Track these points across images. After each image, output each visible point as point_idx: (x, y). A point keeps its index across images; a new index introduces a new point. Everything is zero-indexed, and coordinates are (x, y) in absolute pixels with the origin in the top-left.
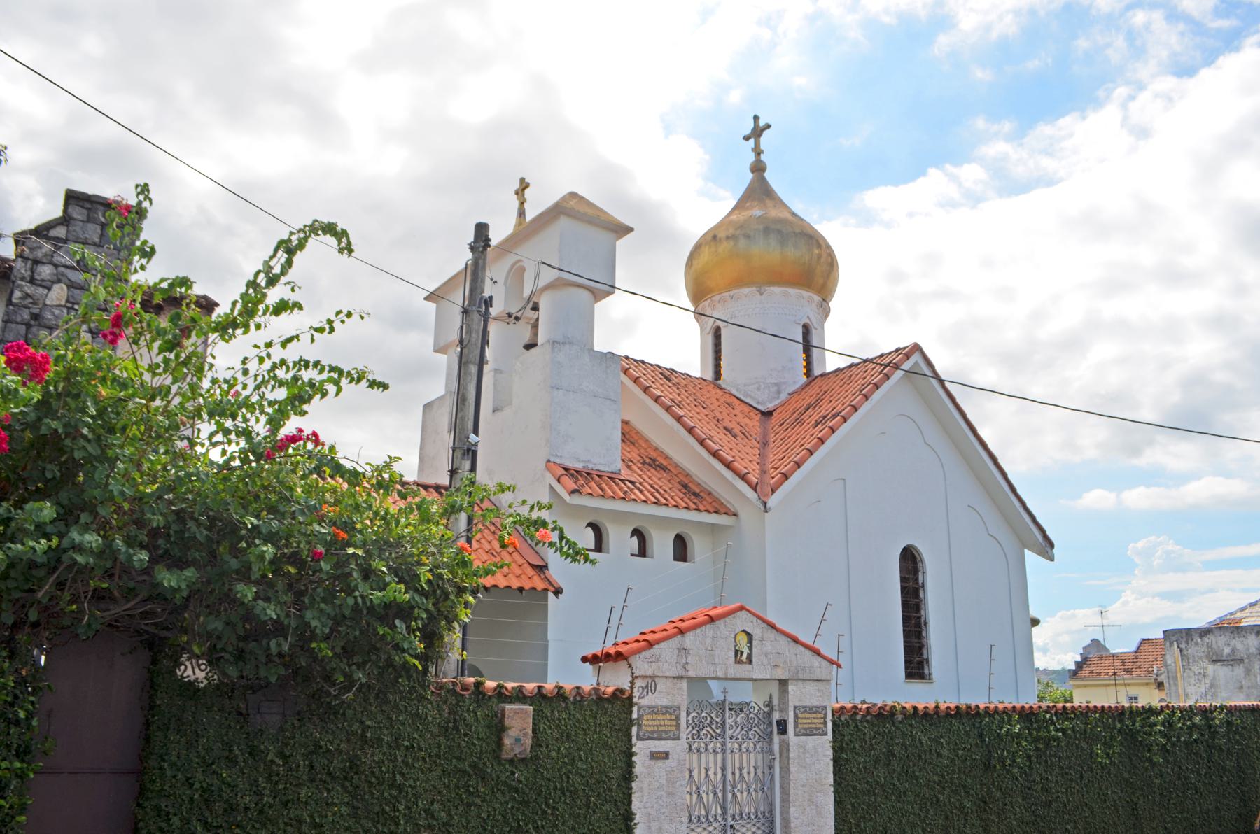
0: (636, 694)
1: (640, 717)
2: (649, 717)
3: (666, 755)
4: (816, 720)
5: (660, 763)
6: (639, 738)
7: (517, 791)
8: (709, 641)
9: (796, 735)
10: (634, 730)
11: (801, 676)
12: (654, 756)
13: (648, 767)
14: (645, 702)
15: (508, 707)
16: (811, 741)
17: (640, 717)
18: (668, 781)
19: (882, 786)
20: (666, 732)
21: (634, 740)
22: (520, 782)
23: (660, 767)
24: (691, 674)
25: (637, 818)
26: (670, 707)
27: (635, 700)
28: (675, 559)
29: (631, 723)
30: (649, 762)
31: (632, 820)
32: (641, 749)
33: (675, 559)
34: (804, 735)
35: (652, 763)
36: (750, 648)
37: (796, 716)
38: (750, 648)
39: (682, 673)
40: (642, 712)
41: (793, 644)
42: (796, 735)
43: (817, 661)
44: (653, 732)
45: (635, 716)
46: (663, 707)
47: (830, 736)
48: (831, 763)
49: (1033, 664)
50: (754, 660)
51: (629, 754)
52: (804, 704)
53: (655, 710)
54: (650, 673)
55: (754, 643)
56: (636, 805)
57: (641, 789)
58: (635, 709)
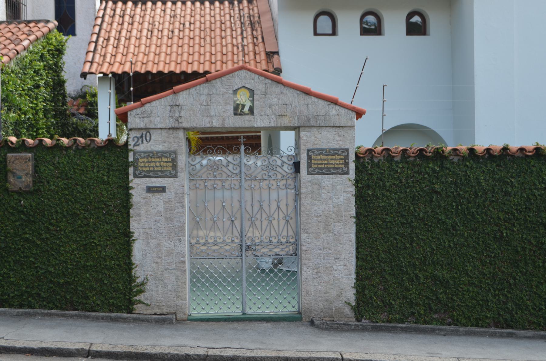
0: (131, 143)
1: (136, 160)
2: (145, 160)
3: (162, 189)
4: (337, 161)
5: (158, 196)
6: (136, 176)
7: (23, 212)
8: (203, 98)
9: (309, 173)
10: (131, 170)
11: (313, 123)
12: (150, 189)
13: (146, 198)
14: (142, 148)
15: (9, 155)
16: (327, 180)
17: (136, 160)
18: (166, 209)
19: (422, 219)
20: (162, 171)
21: (131, 177)
22: (25, 207)
23: (157, 199)
24: (185, 125)
25: (135, 236)
26: (166, 152)
27: (130, 147)
28: (361, 34)
29: (127, 165)
30: (145, 194)
31: (130, 237)
32: (138, 186)
33: (361, 34)
34: (318, 173)
35: (150, 195)
36: (253, 101)
37: (309, 158)
38: (253, 101)
39: (177, 125)
40: (137, 156)
41: (302, 96)
42: (309, 173)
43: (333, 110)
44: (149, 172)
45: (131, 159)
46: (157, 152)
47: (352, 175)
48: (353, 199)
49: (282, 130)
50: (255, 111)
51: (127, 188)
52: (318, 147)
53: (150, 155)
54: (142, 125)
55: (256, 97)
56: (134, 225)
57: (139, 215)
58: (131, 154)
